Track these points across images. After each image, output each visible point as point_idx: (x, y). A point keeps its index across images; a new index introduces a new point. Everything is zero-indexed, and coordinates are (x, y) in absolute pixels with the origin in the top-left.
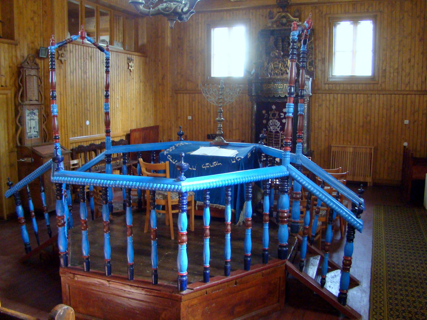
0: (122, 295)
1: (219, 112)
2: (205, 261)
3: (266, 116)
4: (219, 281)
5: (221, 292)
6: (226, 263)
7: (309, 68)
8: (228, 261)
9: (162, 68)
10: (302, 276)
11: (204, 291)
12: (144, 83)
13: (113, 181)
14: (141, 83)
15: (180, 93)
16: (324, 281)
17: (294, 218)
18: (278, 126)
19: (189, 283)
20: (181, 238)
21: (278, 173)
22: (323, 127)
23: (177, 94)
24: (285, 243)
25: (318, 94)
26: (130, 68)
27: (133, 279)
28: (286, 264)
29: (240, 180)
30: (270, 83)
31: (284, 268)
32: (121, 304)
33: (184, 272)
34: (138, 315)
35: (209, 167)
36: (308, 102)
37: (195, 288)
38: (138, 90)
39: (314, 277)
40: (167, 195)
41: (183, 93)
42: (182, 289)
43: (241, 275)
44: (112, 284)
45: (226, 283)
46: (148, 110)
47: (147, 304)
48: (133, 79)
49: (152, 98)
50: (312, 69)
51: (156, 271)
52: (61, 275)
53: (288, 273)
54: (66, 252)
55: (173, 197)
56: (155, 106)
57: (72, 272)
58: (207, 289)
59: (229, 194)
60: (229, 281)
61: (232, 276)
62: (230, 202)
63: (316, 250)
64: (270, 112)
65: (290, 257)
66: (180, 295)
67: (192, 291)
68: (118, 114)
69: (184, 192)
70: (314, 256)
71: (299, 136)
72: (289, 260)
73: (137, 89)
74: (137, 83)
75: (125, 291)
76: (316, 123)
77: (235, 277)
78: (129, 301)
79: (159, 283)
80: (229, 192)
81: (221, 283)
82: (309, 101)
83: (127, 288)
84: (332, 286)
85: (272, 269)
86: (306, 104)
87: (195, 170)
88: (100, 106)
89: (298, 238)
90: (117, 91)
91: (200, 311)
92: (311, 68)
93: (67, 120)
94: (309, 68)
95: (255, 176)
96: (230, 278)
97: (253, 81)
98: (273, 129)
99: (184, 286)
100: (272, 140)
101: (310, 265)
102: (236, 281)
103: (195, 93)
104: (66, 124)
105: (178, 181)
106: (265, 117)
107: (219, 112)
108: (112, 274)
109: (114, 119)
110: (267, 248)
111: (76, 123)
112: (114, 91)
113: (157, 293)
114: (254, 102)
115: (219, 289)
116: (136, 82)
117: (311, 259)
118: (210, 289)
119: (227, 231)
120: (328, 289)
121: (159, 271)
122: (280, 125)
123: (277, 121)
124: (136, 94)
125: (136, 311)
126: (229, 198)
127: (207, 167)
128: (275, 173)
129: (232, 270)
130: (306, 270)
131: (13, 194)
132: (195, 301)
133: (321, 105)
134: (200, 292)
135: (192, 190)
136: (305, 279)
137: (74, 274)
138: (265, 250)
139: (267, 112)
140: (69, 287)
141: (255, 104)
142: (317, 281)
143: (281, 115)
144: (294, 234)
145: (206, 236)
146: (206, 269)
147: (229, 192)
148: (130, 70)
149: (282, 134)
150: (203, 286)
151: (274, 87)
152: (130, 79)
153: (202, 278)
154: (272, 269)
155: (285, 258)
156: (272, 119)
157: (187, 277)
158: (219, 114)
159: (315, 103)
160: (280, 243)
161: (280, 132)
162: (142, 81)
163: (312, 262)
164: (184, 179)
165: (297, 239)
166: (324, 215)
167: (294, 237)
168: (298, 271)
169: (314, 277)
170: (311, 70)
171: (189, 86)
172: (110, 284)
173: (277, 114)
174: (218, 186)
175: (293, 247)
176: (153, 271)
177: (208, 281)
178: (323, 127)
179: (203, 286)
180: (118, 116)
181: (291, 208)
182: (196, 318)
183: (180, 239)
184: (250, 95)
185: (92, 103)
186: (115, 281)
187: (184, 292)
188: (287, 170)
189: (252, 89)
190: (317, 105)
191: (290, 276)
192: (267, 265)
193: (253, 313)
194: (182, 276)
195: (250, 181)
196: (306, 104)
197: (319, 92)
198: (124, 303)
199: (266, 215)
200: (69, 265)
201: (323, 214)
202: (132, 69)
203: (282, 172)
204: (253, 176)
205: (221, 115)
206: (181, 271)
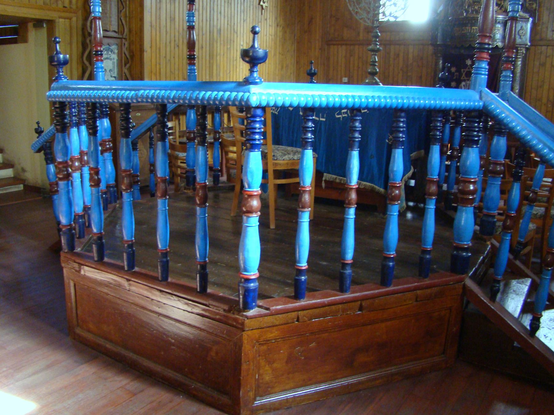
0: (148, 307)
1: (373, 37)
2: (299, 256)
3: (456, 75)
4: (326, 300)
5: (330, 321)
6: (344, 265)
7: (530, 4)
8: (346, 262)
9: (310, 7)
10: (493, 310)
11: (294, 314)
12: (283, 28)
13: (135, 90)
14: (278, 29)
15: (334, 45)
16: (537, 323)
17: (488, 209)
19: (262, 296)
20: (248, 202)
21: (460, 100)
22: (544, 100)
23: (329, 45)
24: (467, 243)
25: (539, 47)
26: (262, 3)
27: (167, 279)
28: (464, 285)
29: (380, 100)
30: (465, 25)
31: (461, 291)
32: (148, 324)
33: (252, 273)
34: (173, 347)
35: (346, 115)
36: (523, 57)
37: (274, 308)
38: (273, 37)
39: (516, 315)
40: (267, 153)
41: (338, 45)
42: (247, 307)
43: (372, 294)
44: (134, 286)
45: (340, 306)
46: (287, 66)
47: (197, 332)
48: (266, 19)
49: (294, 51)
50: (534, 6)
51: (204, 267)
52: (63, 265)
53: (468, 302)
54: (70, 225)
55: (277, 157)
56: (298, 63)
57: (78, 261)
58: (301, 313)
59: (356, 127)
60: (346, 303)
61: (353, 293)
62: (357, 144)
63: (522, 267)
64: (462, 70)
65: (474, 272)
66: (241, 318)
67: (268, 312)
68: (241, 67)
69: (254, 106)
70: (519, 279)
71: (508, 57)
72: (472, 278)
73: (272, 35)
74: (272, 26)
75: (152, 300)
76: (534, 92)
77: (358, 296)
78: (160, 319)
79: (209, 290)
80: (357, 124)
81: (330, 304)
82: (526, 54)
83: (155, 295)
84: (549, 335)
85: (435, 289)
86: (520, 59)
87: (323, 121)
88: (215, 53)
89: (492, 245)
90: (242, 35)
91: (284, 352)
92: (533, 4)
93: (160, 64)
94: (530, 4)
95: (413, 98)
96: (348, 296)
97: (439, 24)
99: (250, 300)
101: (511, 293)
102: (361, 305)
103: (354, 45)
104: (158, 69)
105: (246, 85)
106: (455, 78)
107: (373, 37)
108: (136, 269)
109: (235, 73)
110: (429, 247)
111: (177, 72)
112: (237, 33)
113: (204, 310)
114: (439, 55)
115: (324, 315)
116: (271, 24)
117: (514, 283)
118: (305, 312)
119: (350, 204)
120: (542, 339)
121: (209, 269)
124: (270, 42)
125: (170, 339)
126: (357, 135)
127: (344, 115)
128: (456, 100)
129: (355, 282)
130: (503, 300)
131: (41, 145)
132: (273, 334)
133: (543, 65)
134: (284, 315)
135: (272, 104)
136: (499, 316)
137: (80, 264)
138: (425, 252)
139: (458, 71)
140: (75, 285)
141: (441, 58)
142: (522, 322)
144: (485, 237)
145: (303, 207)
146: (300, 272)
147: (357, 124)
148: (262, 6)
150: (290, 306)
151: (471, 31)
152: (261, 19)
153: (290, 291)
154: (435, 289)
155: (464, 271)
156: (464, 81)
157: (257, 284)
158: (374, 39)
159: (534, 61)
160: (457, 243)
162: (279, 24)
163: (515, 288)
164: (258, 81)
165: (490, 246)
166: (541, 215)
167: (485, 241)
168: (488, 300)
169: (516, 315)
170: (532, 8)
171: (347, 34)
172: (130, 285)
174: (331, 105)
175: (482, 257)
176: (199, 266)
177: (303, 298)
178: (544, 100)
179: (290, 306)
180: (241, 70)
181: (483, 193)
182: (275, 365)
183: (245, 205)
184: (434, 45)
185: (202, 47)
186: (137, 281)
187: (251, 313)
188: (481, 98)
189: (436, 36)
190: (537, 63)
191: (471, 306)
192: (427, 281)
193: (393, 369)
194: (248, 280)
195: (400, 106)
196: (520, 59)
197: (541, 43)
198: (153, 323)
199: (432, 181)
200: (78, 250)
201: (539, 214)
202: (264, 5)
203: (470, 101)
204: (408, 98)
205: (376, 41)
206: (246, 270)
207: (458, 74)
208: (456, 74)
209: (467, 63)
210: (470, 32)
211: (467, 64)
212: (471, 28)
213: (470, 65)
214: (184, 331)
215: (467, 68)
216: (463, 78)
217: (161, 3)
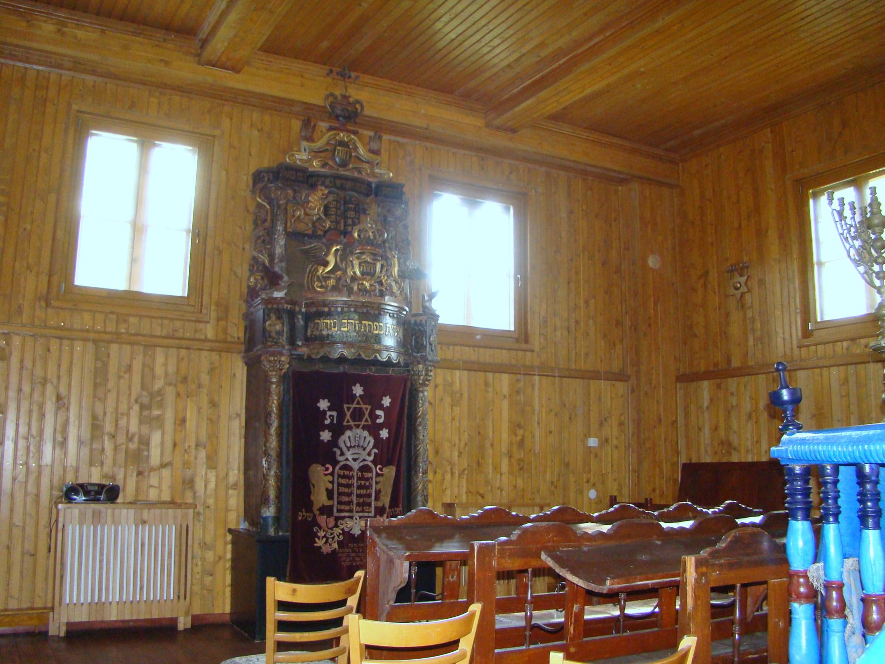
18: (368, 450)
64: (345, 406)
98: (355, 460)
100: (349, 495)
106: (327, 422)
122: (374, 447)
123: (366, 433)
143: (378, 417)
149: (378, 475)
161: (373, 467)
173: (367, 413)
207: (334, 413)
208: (329, 413)
209: (354, 392)
210: (360, 331)
211: (355, 394)
212: (361, 323)
213: (360, 396)
214: (865, 471)
215: (349, 424)
216: (348, 421)
217: (127, 506)
